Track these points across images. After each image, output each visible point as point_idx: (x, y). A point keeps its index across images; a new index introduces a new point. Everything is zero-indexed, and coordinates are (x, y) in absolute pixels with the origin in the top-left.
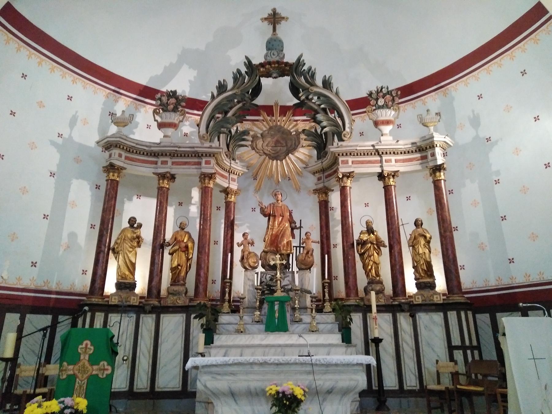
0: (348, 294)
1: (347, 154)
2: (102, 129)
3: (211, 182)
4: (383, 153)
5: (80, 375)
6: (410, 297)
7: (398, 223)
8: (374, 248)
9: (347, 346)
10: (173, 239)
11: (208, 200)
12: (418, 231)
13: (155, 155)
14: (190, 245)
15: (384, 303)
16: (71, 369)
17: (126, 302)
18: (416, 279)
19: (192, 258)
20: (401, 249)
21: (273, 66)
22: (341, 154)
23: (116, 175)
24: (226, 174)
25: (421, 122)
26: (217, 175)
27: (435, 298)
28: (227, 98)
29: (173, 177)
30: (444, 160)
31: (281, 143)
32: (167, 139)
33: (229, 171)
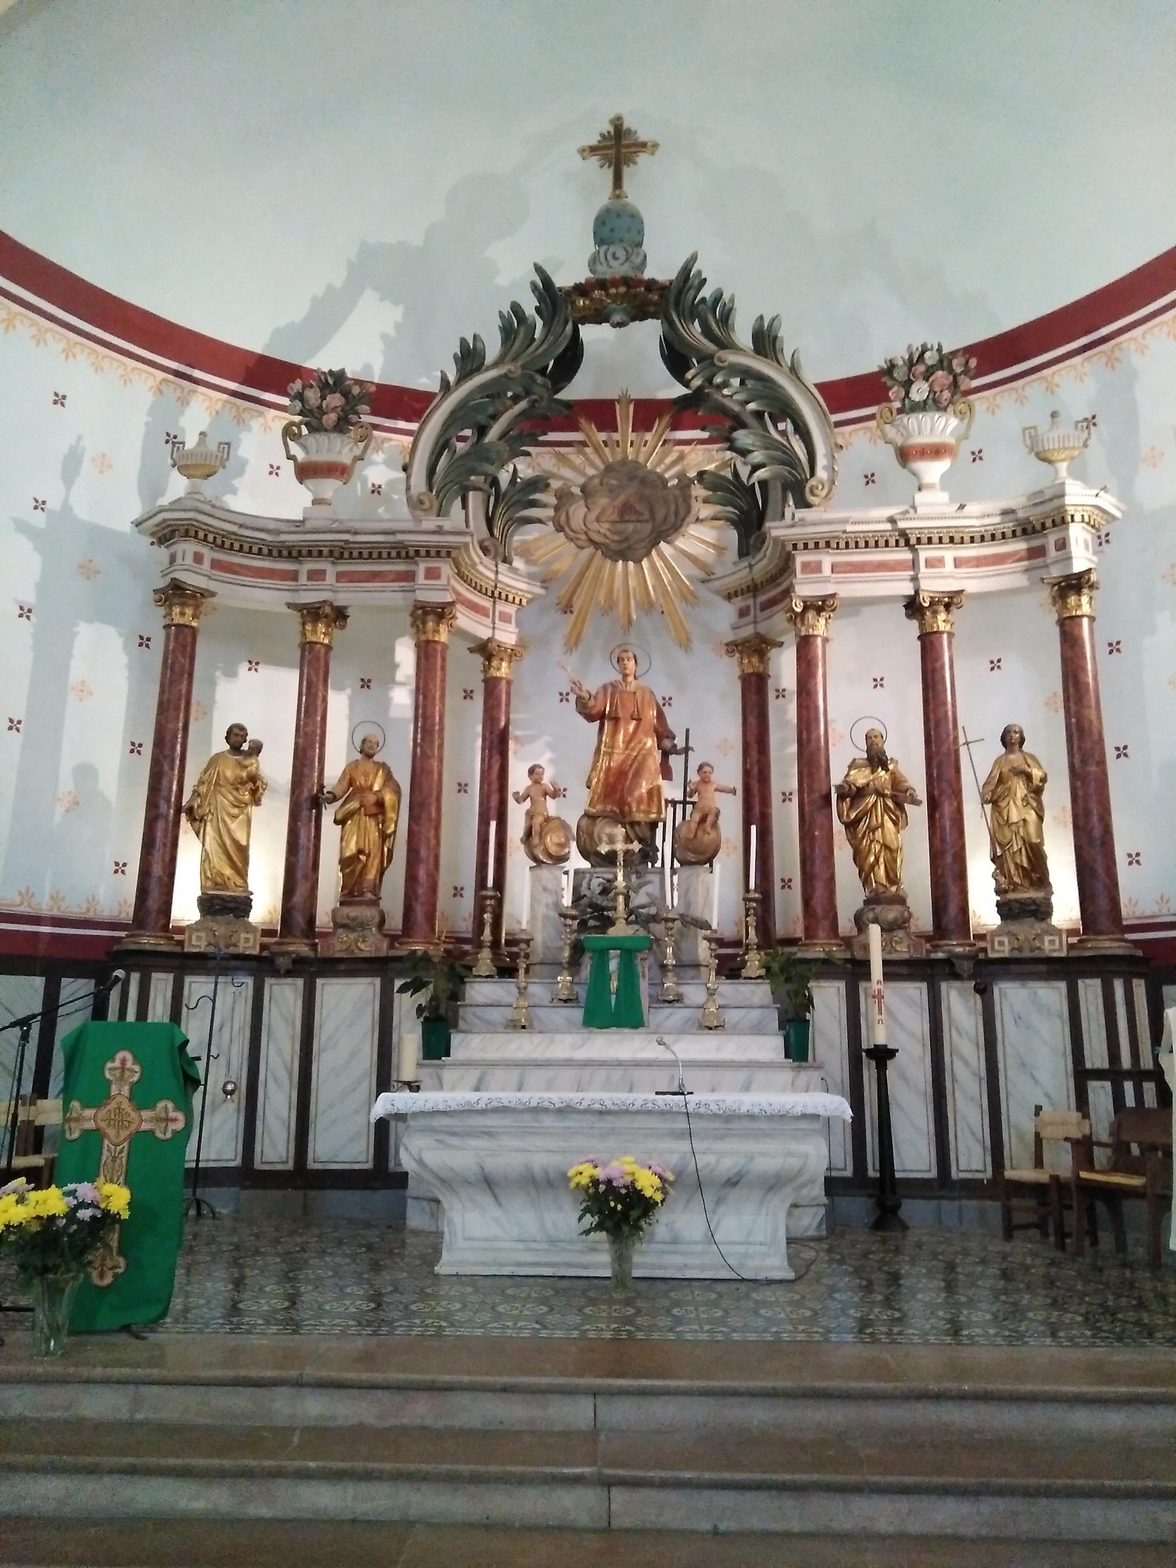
0: (810, 932)
1: (817, 545)
2: (150, 486)
3: (443, 628)
4: (919, 540)
5: (111, 1132)
6: (981, 937)
7: (956, 738)
8: (886, 808)
9: (798, 1067)
10: (345, 783)
11: (435, 676)
12: (1011, 761)
13: (290, 556)
14: (389, 798)
15: (906, 956)
16: (89, 1118)
17: (227, 946)
18: (998, 892)
19: (395, 832)
20: (959, 811)
21: (613, 291)
22: (800, 546)
23: (189, 611)
24: (486, 603)
25: (1032, 449)
26: (458, 606)
27: (1046, 943)
28: (483, 387)
29: (340, 615)
30: (1095, 559)
31: (637, 512)
32: (322, 511)
33: (493, 592)
